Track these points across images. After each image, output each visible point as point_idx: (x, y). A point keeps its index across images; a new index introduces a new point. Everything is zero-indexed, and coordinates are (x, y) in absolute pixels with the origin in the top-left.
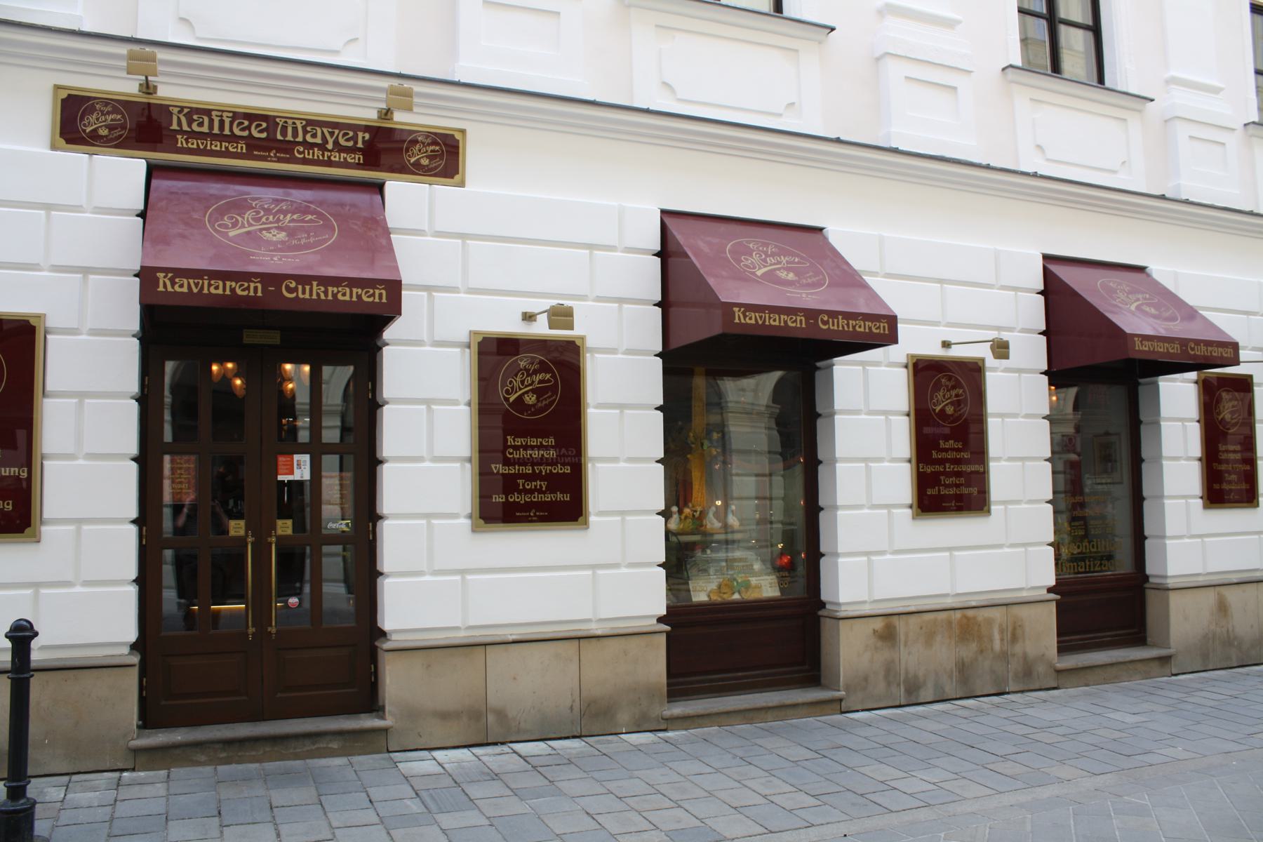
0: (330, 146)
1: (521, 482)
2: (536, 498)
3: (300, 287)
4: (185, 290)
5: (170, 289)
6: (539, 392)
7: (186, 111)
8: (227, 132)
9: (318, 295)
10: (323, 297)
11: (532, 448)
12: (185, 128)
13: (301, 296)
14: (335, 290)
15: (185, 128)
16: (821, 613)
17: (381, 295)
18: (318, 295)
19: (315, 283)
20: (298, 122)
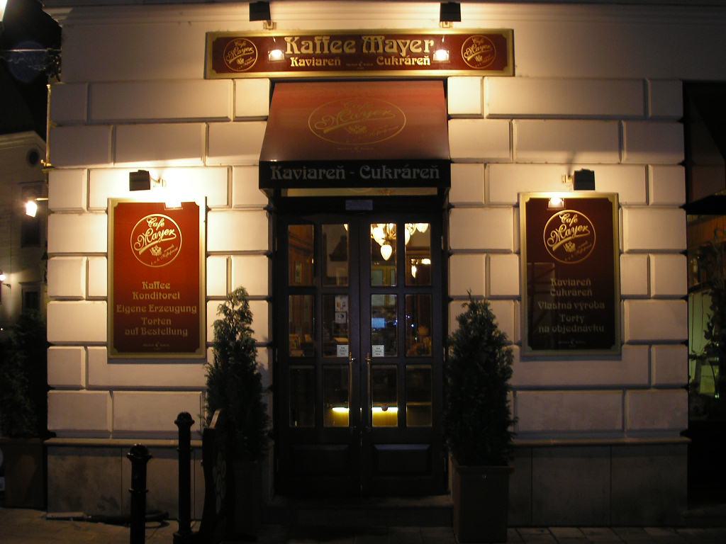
0: (403, 54)
1: (144, 319)
2: (575, 329)
3: (373, 170)
4: (290, 177)
5: (280, 178)
6: (164, 246)
7: (296, 39)
8: (326, 51)
9: (387, 175)
10: (390, 177)
11: (572, 288)
12: (297, 52)
13: (374, 177)
14: (400, 171)
15: (297, 52)
16: (510, 429)
17: (435, 173)
18: (387, 175)
19: (384, 167)
20: (378, 38)
